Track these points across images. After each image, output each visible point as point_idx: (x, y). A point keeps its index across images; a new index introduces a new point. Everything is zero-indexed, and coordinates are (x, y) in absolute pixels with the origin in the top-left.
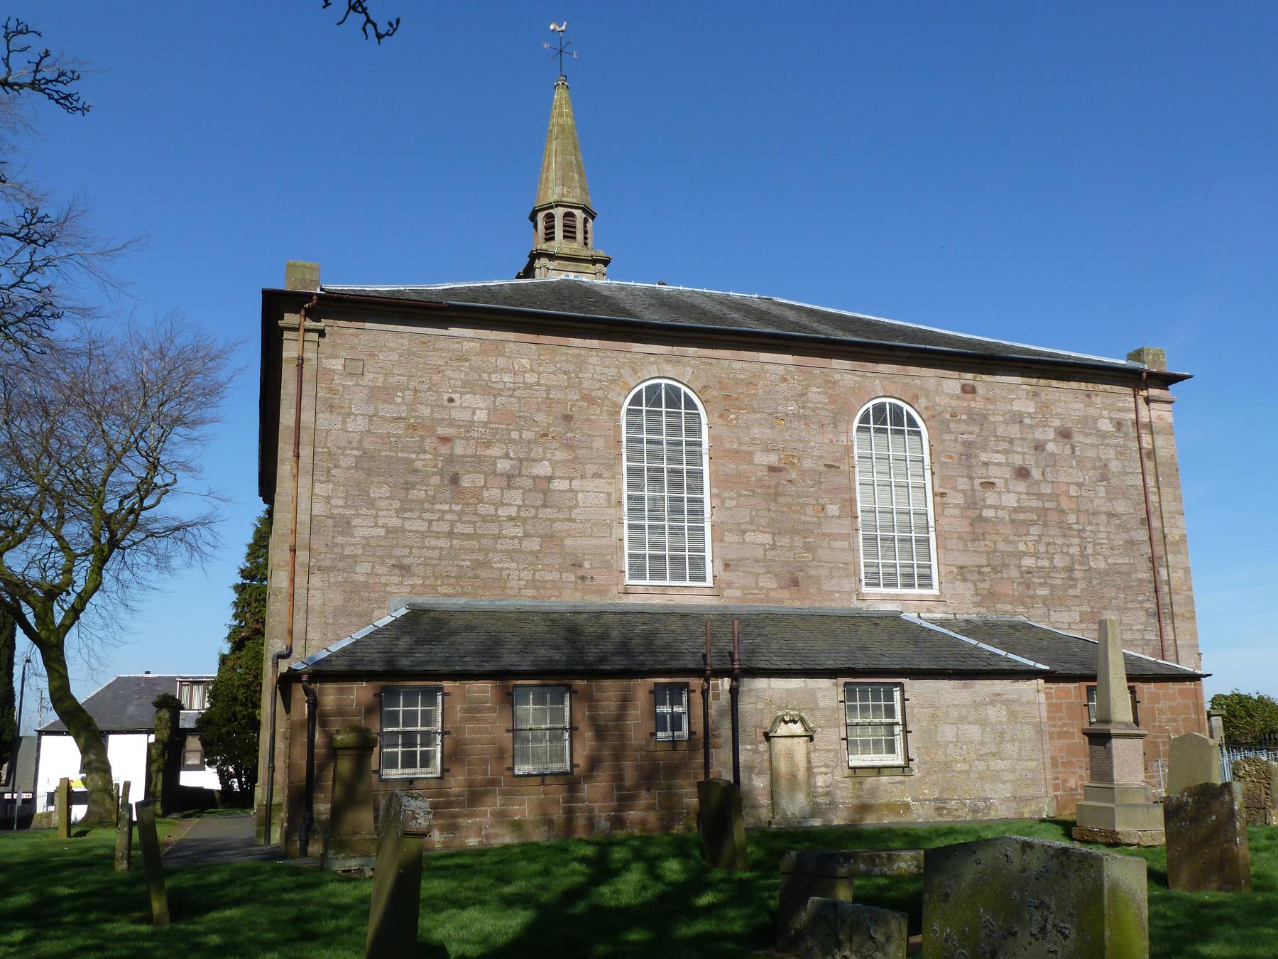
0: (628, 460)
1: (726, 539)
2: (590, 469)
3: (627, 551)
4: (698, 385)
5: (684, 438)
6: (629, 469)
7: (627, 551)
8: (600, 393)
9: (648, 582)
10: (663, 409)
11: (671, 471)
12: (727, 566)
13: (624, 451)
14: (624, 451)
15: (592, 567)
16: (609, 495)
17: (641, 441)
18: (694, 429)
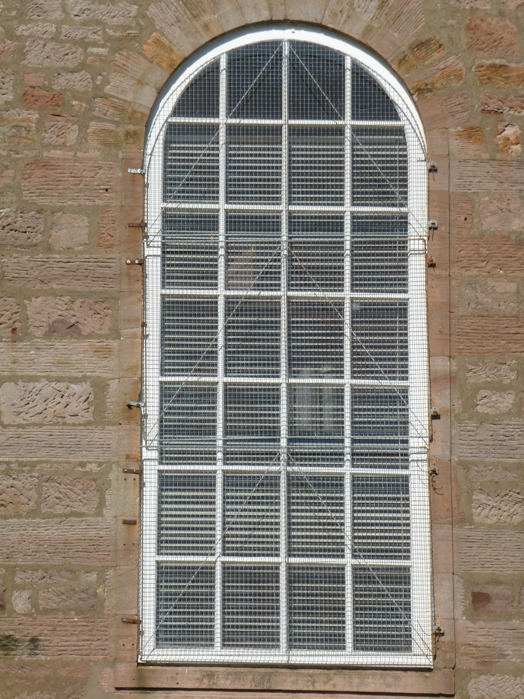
0: (166, 280)
1: (480, 515)
2: (42, 310)
3: (150, 558)
4: (401, 39)
5: (347, 208)
6: (168, 306)
7: (150, 558)
8: (80, 81)
9: (217, 653)
10: (222, 119)
11: (364, 312)
12: (479, 600)
13: (153, 253)
14: (153, 253)
15: (36, 610)
16: (100, 386)
17: (209, 222)
18: (384, 180)
